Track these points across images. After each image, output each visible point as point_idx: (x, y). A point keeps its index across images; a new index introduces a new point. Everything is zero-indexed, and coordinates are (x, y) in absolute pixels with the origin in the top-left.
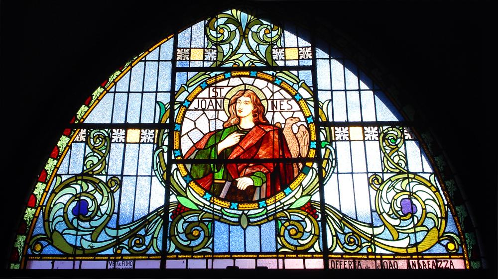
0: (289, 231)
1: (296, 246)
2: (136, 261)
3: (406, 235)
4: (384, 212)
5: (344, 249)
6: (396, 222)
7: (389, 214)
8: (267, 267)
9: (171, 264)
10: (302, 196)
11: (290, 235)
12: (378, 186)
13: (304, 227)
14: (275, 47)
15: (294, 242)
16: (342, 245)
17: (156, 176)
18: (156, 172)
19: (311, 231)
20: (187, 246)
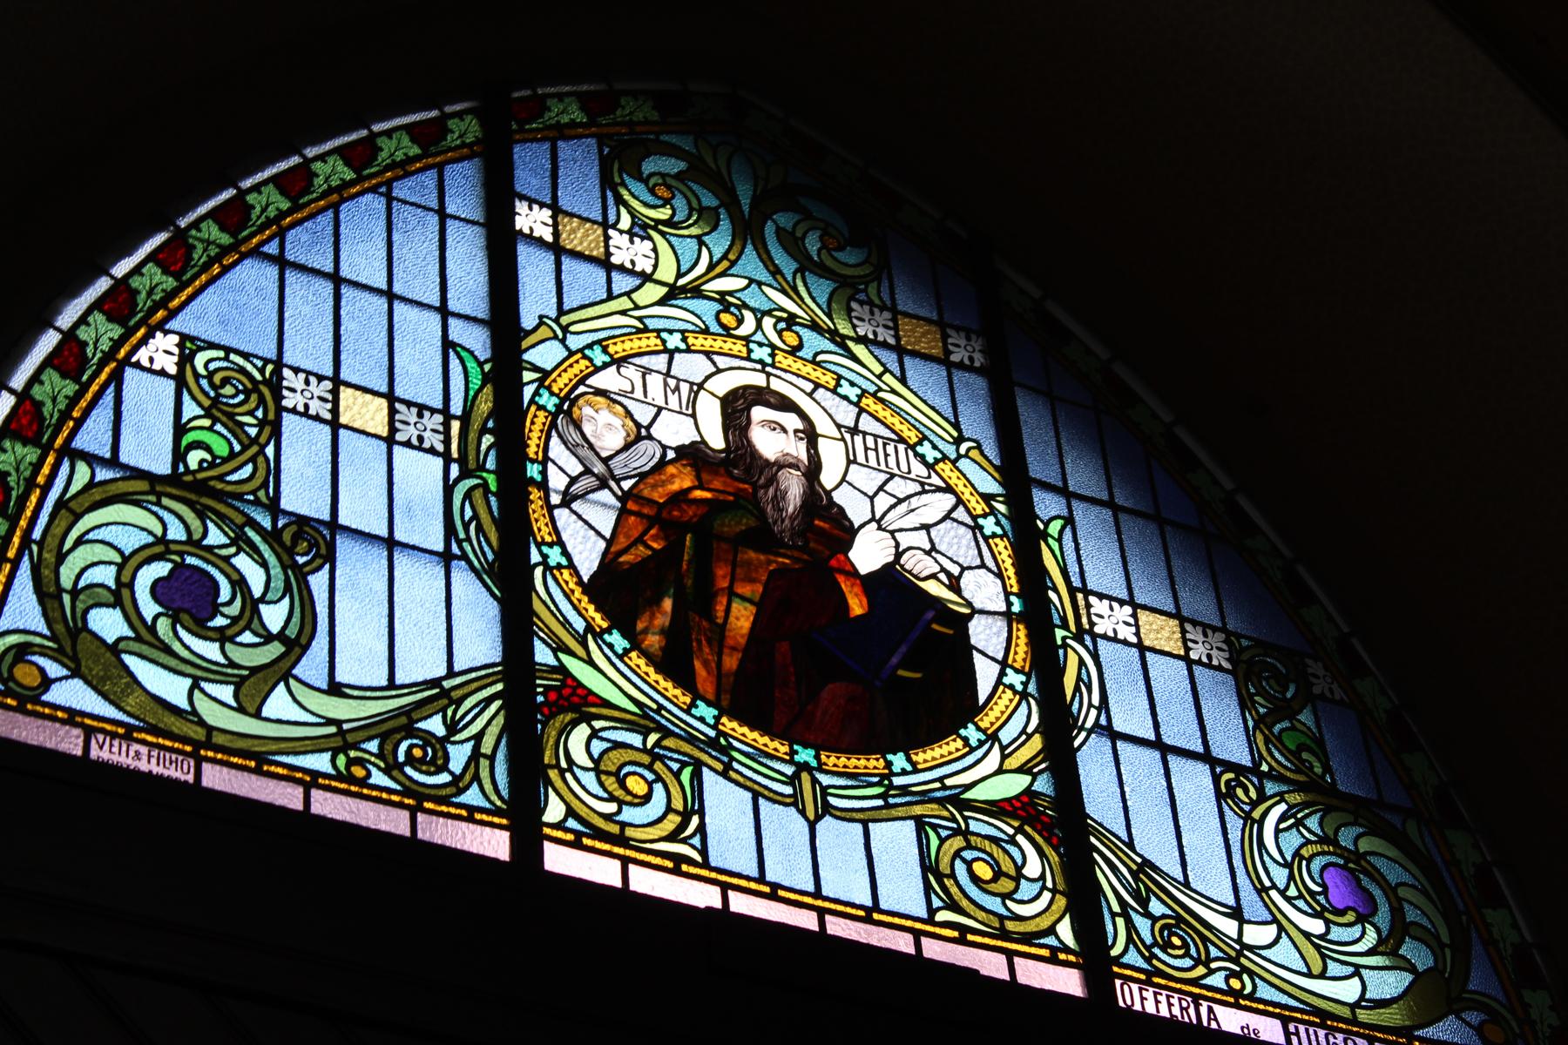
0: (969, 864)
1: (1001, 918)
2: (384, 683)
3: (1351, 970)
4: (1274, 886)
5: (1155, 962)
6: (1317, 926)
7: (1288, 893)
8: (978, 971)
9: (934, 950)
10: (1000, 771)
11: (975, 879)
12: (1247, 808)
13: (1019, 862)
14: (862, 296)
15: (994, 904)
16: (1148, 948)
17: (464, 557)
18: (466, 545)
19: (1042, 877)
20: (608, 817)
